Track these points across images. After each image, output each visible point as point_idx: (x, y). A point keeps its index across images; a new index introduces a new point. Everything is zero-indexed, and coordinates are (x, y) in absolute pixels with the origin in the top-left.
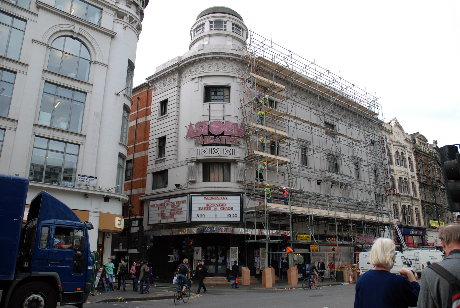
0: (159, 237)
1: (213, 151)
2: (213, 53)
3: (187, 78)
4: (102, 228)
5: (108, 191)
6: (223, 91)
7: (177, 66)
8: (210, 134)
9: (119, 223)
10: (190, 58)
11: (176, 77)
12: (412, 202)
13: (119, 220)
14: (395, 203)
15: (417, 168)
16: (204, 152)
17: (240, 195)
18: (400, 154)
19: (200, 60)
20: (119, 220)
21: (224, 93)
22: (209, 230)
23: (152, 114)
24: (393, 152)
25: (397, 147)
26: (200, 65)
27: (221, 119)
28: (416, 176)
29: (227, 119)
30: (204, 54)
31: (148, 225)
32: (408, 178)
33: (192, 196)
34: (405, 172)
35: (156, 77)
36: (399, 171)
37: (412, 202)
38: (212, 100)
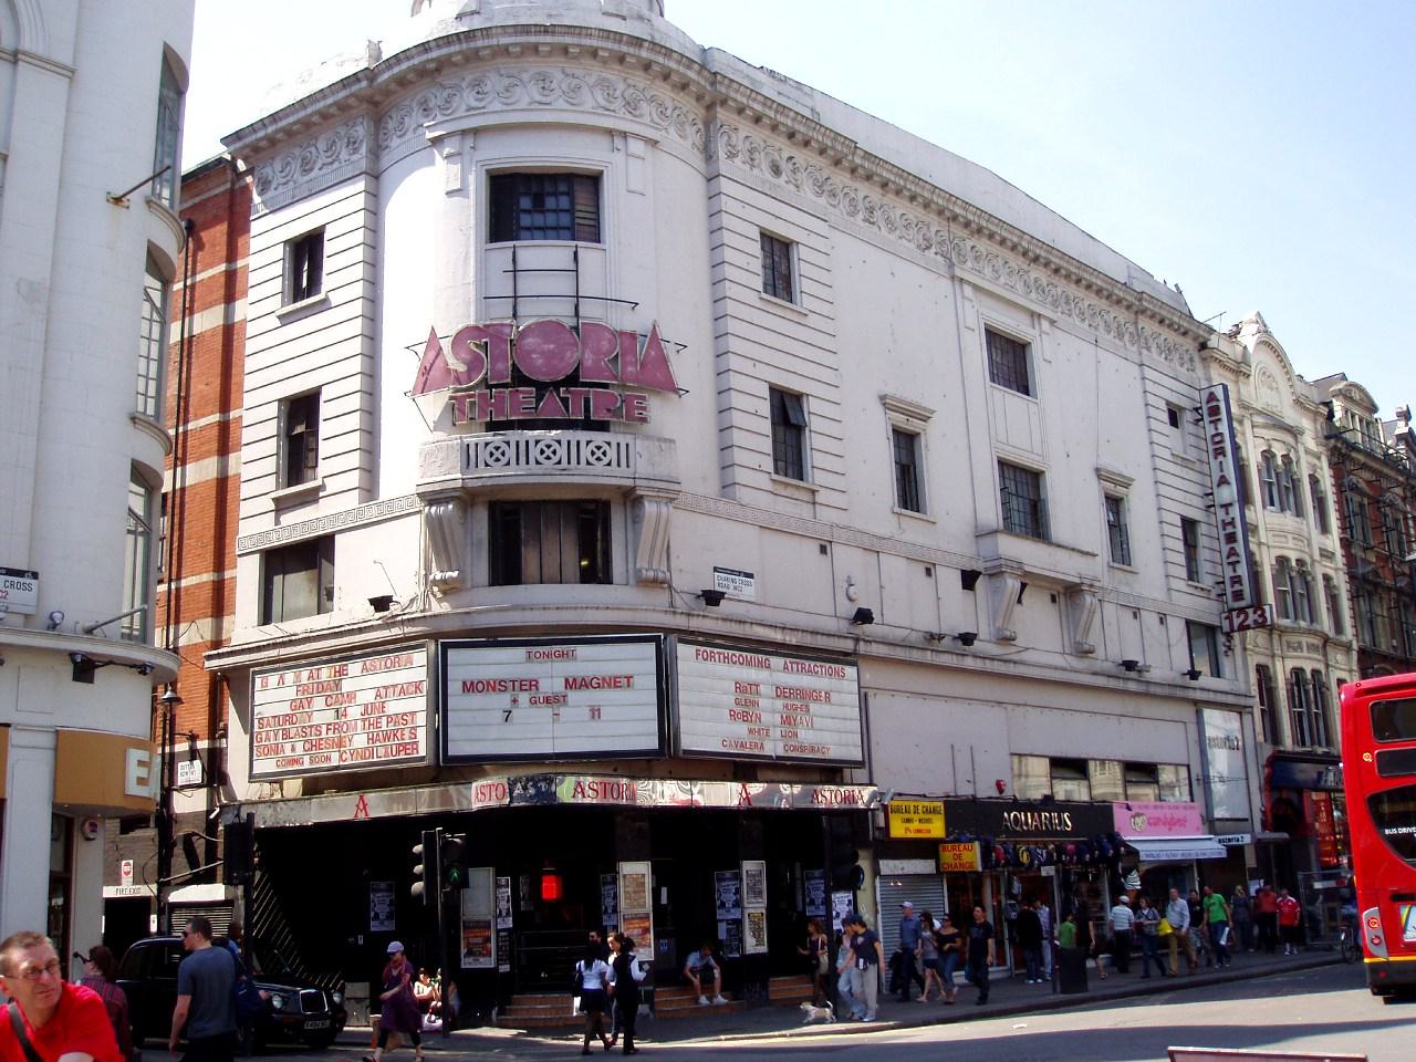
0: (303, 828)
1: (534, 452)
2: (525, 29)
3: (410, 135)
4: (67, 799)
5: (90, 631)
6: (570, 194)
7: (364, 84)
8: (519, 379)
9: (143, 772)
10: (424, 47)
11: (361, 130)
12: (1325, 655)
13: (141, 763)
14: (1263, 660)
15: (1343, 518)
16: (496, 455)
17: (656, 640)
18: (1279, 462)
19: (473, 57)
20: (141, 763)
21: (572, 203)
22: (532, 791)
23: (253, 295)
24: (1253, 457)
25: (1269, 434)
26: (469, 78)
27: (562, 311)
28: (1339, 552)
29: (590, 311)
30: (486, 32)
31: (252, 778)
32: (1308, 560)
33: (445, 647)
34: (1300, 538)
35: (270, 129)
36: (1279, 535)
37: (1325, 655)
38: (523, 233)
